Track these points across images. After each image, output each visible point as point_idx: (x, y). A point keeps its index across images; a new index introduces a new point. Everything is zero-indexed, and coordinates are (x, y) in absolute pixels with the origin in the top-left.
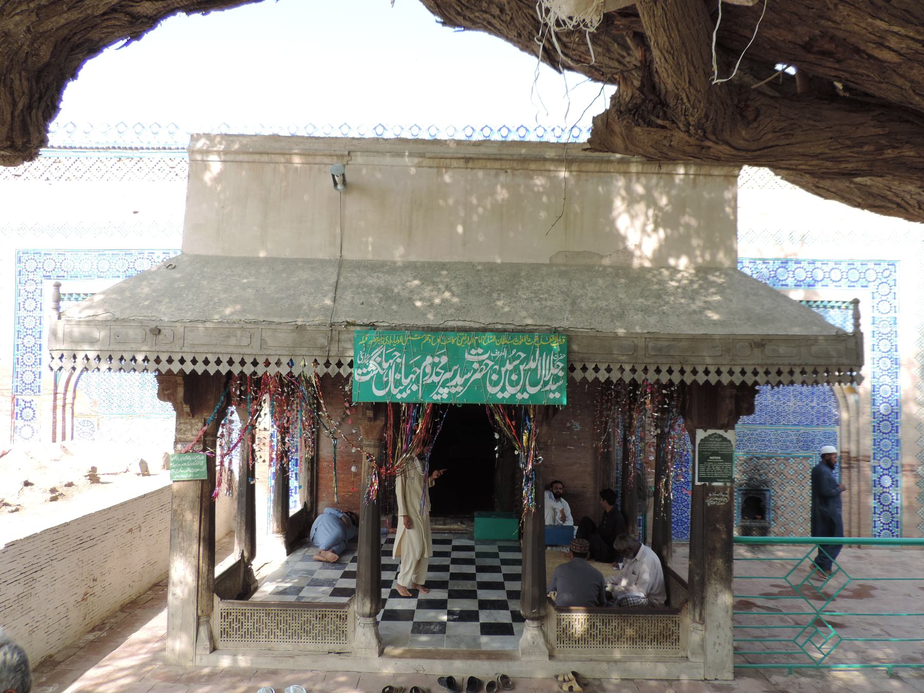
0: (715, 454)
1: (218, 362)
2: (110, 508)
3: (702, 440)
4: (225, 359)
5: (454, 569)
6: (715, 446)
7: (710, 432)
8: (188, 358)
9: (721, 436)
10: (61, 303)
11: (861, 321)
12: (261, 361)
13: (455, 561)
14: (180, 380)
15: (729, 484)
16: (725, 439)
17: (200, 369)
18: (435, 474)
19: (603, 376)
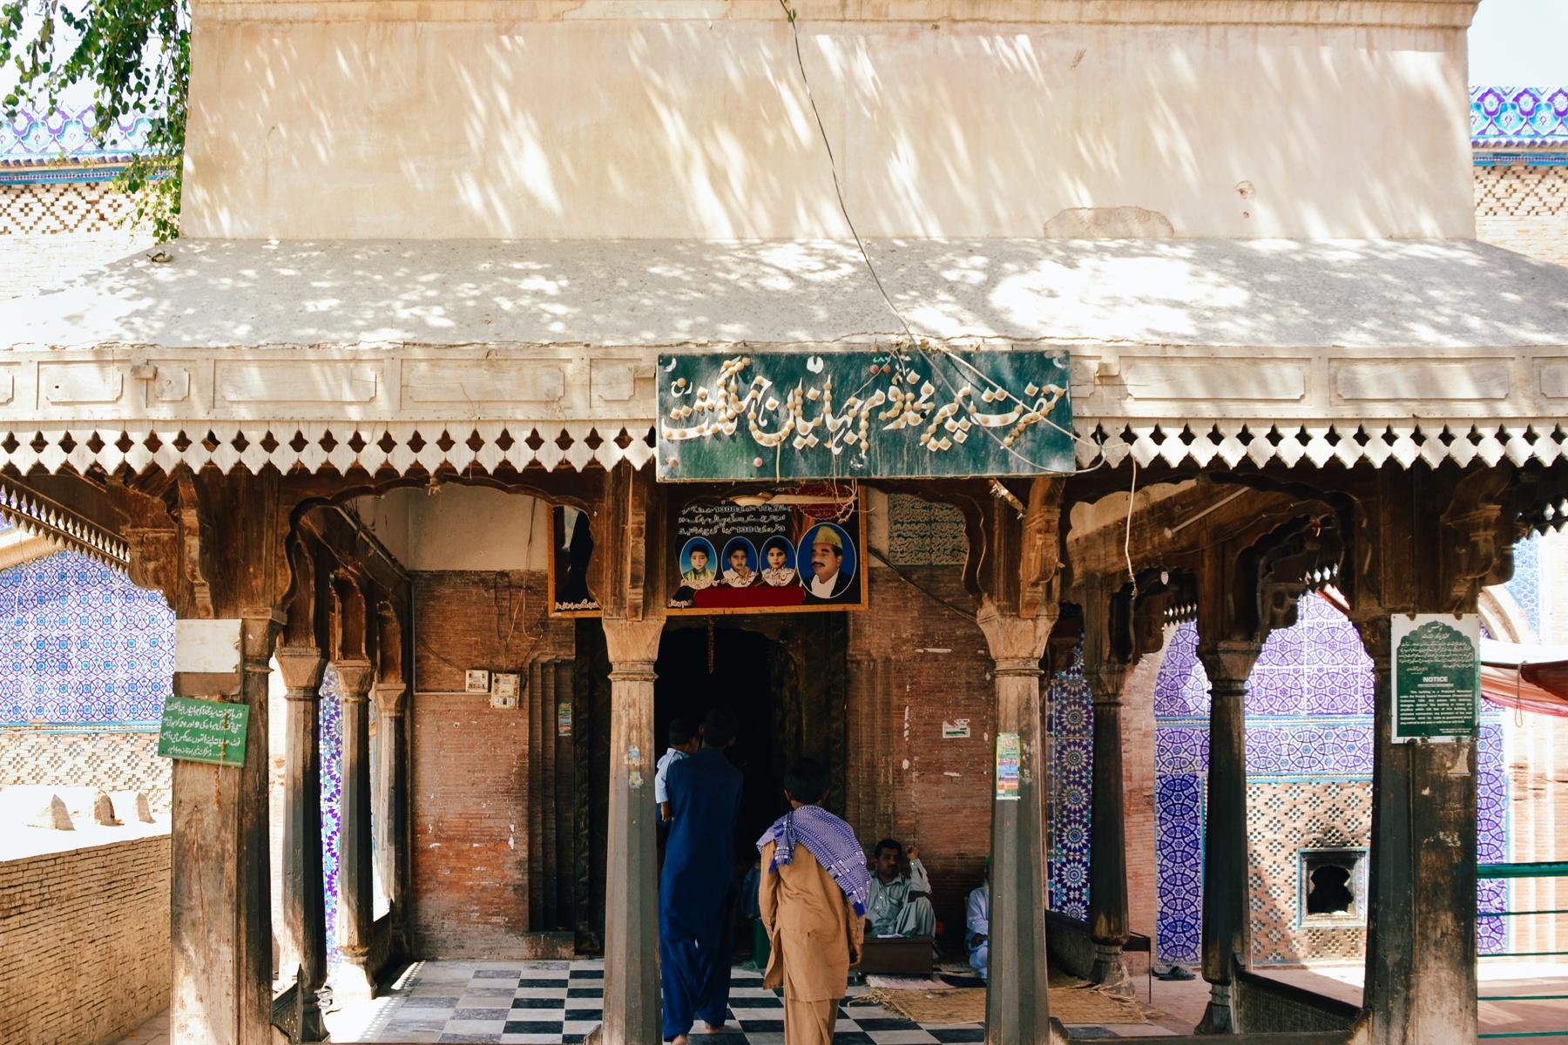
0: (1435, 670)
1: (299, 443)
2: (77, 853)
3: (1404, 640)
4: (314, 436)
5: (557, 1015)
6: (1434, 650)
7: (1423, 619)
8: (460, 435)
9: (1448, 629)
10: (1150, 370)
11: (190, 78)
12: (402, 437)
13: (574, 993)
14: (187, 491)
15: (1466, 739)
16: (1457, 636)
17: (226, 459)
18: (671, 755)
19: (642, 453)
